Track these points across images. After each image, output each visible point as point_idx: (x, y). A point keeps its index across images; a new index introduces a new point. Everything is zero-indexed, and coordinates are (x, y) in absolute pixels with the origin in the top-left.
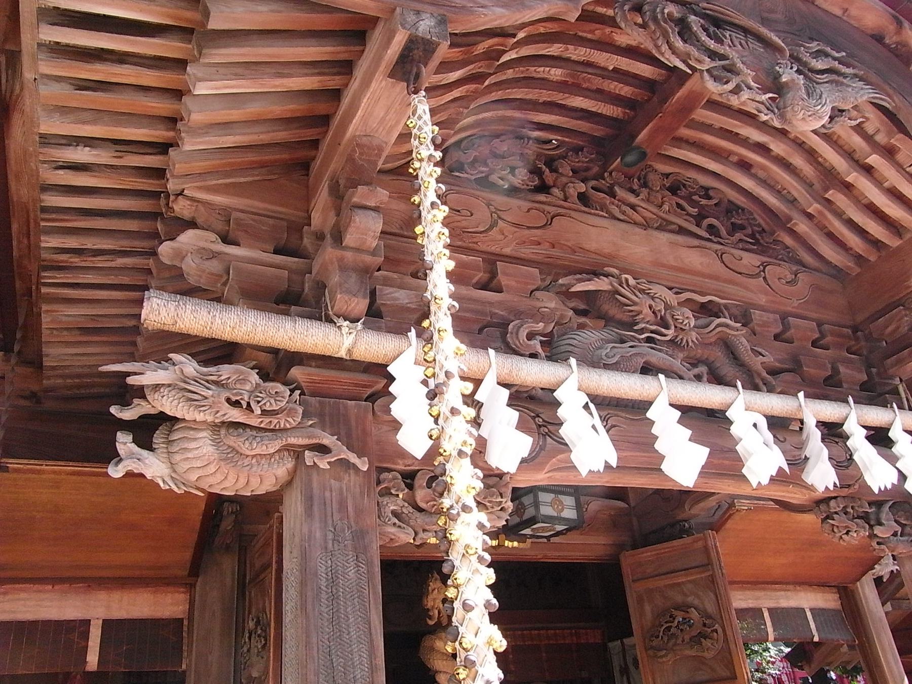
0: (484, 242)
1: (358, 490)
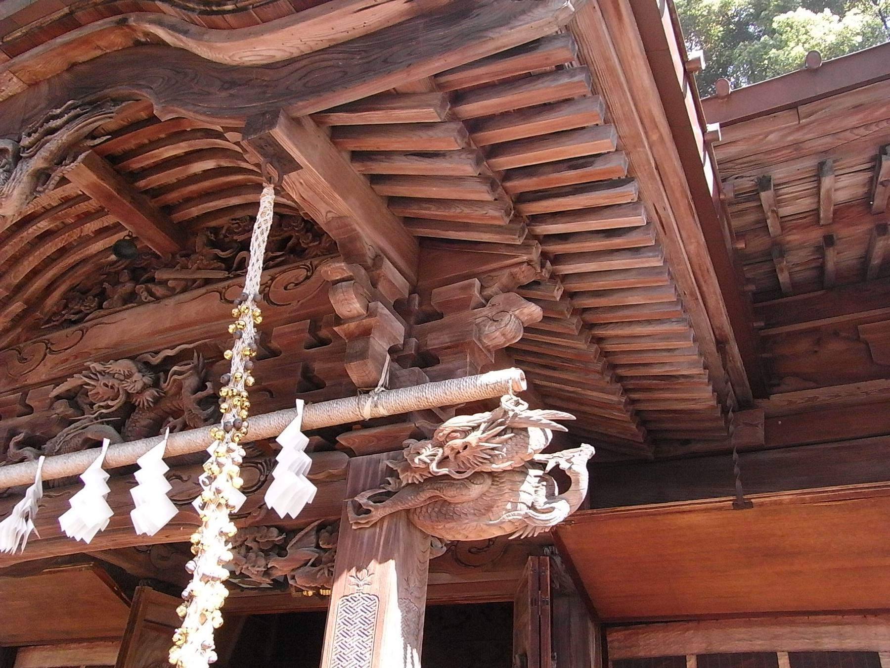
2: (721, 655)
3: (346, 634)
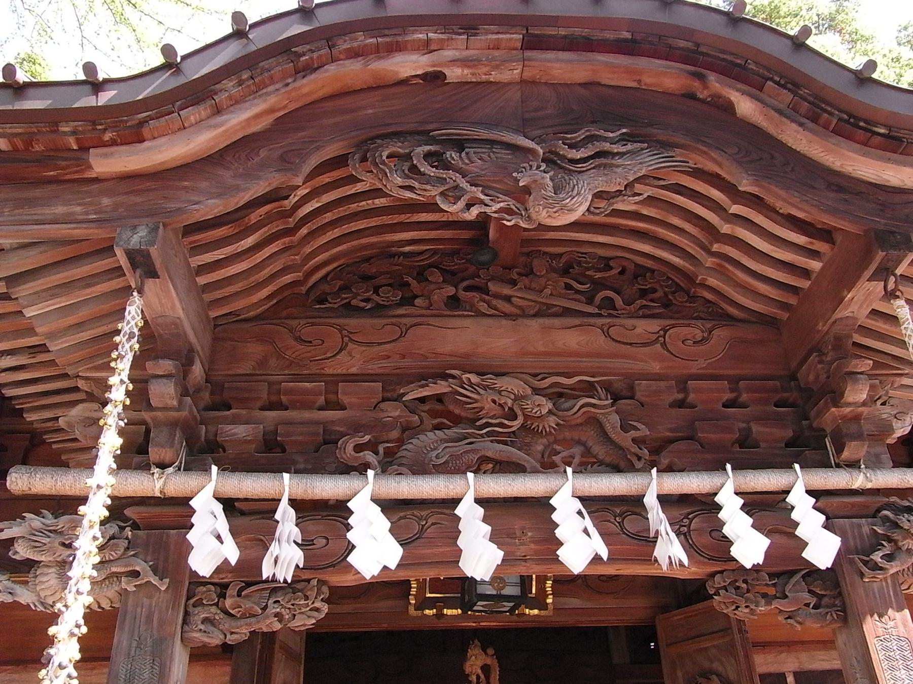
0: (330, 367)
1: (165, 604)
2: (812, 672)
3: (892, 669)
